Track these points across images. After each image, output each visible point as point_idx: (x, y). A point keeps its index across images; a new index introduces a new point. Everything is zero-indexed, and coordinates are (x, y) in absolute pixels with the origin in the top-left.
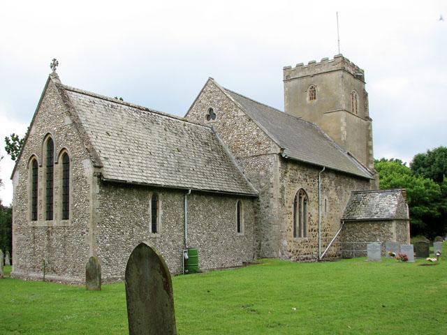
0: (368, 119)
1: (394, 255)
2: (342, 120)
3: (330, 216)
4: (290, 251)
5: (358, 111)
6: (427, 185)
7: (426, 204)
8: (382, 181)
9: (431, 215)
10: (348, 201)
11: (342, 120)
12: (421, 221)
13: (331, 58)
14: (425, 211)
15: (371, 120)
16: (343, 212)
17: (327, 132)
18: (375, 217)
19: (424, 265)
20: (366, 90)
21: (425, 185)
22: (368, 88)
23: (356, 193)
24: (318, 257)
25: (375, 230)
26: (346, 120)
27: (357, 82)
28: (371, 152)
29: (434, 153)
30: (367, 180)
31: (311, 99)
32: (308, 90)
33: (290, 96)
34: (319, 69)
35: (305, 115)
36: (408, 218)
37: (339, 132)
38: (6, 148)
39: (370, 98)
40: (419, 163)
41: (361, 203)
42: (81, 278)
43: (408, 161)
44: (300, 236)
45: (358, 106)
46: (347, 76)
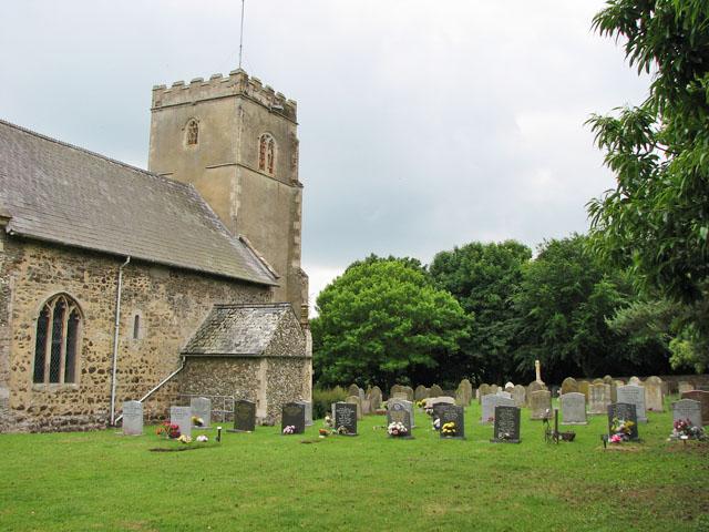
0: (295, 183)
1: (200, 424)
2: (234, 181)
3: (149, 347)
4: (21, 408)
5: (274, 168)
6: (439, 301)
7: (439, 331)
8: (371, 291)
9: (446, 349)
10: (203, 320)
11: (234, 181)
12: (428, 358)
13: (226, 76)
14: (434, 342)
15: (301, 186)
16: (189, 339)
17: (209, 200)
18: (234, 352)
19: (155, 450)
20: (298, 137)
21: (436, 301)
22: (300, 133)
23: (220, 307)
24: (109, 419)
25: (233, 375)
26: (241, 181)
27: (276, 120)
28: (297, 239)
29: (462, 252)
30: (265, 288)
31: (190, 142)
32: (187, 127)
33: (162, 141)
34: (205, 93)
35: (177, 170)
36: (311, 354)
37: (227, 202)
38: (407, 259)
39: (301, 148)
40: (444, 264)
41: (222, 326)
42: (648, 407)
43: (427, 260)
44: (54, 378)
45: (275, 160)
46: (252, 109)
